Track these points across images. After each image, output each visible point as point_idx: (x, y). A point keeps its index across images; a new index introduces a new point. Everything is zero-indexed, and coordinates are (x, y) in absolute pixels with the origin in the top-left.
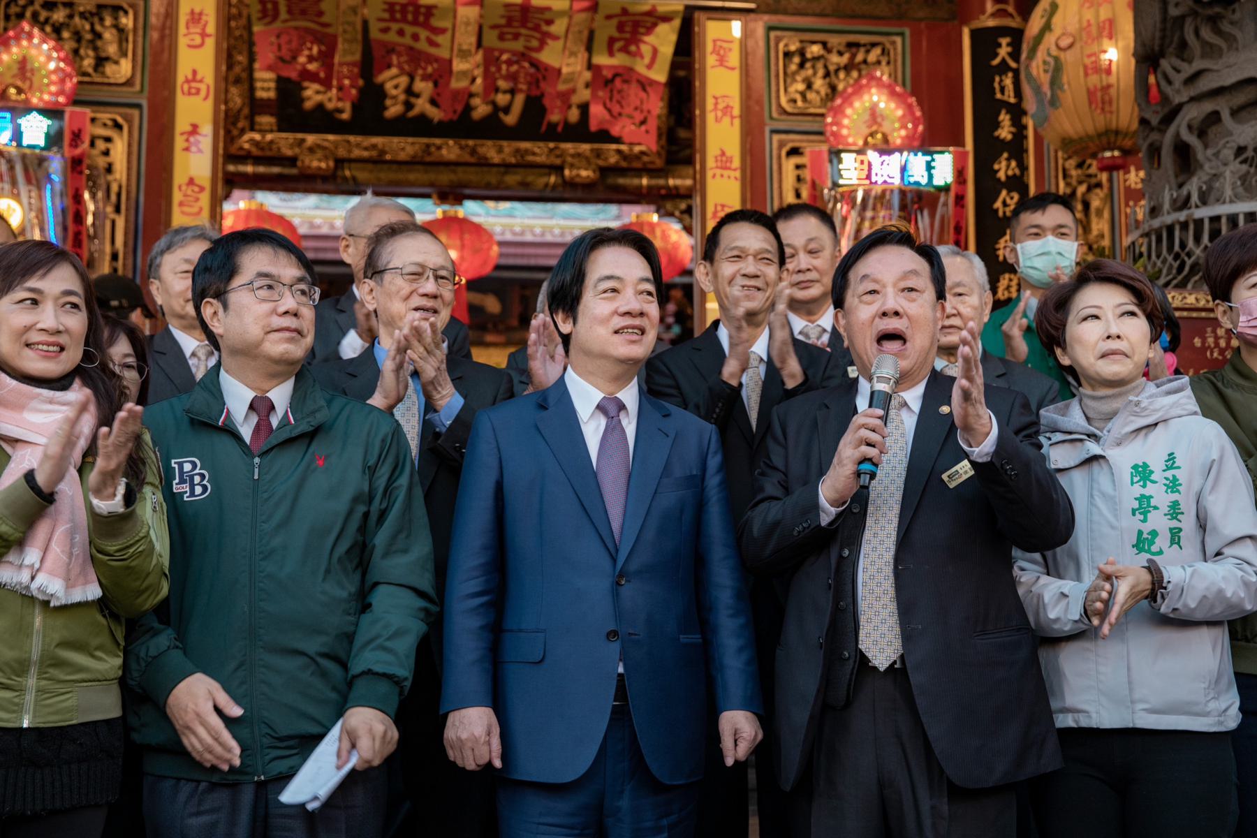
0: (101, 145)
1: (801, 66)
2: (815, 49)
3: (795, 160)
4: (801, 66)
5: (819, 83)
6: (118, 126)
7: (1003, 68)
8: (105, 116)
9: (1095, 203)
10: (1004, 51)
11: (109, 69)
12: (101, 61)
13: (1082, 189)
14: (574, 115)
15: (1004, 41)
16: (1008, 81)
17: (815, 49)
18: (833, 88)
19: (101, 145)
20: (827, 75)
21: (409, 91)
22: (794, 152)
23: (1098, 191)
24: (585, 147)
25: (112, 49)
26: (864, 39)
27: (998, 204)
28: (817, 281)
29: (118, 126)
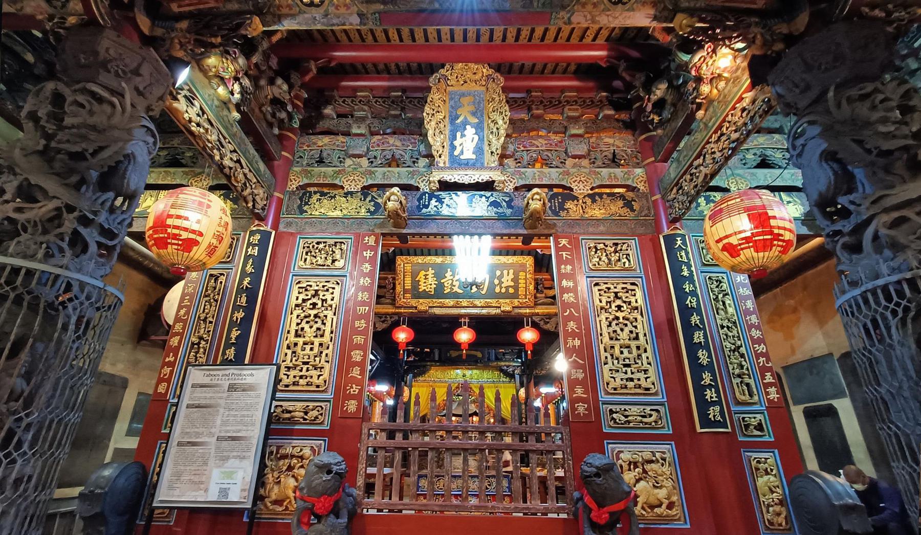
0: (331, 290)
1: (596, 252)
2: (602, 246)
3: (597, 288)
4: (596, 252)
5: (604, 258)
6: (338, 284)
7: (680, 248)
8: (333, 280)
9: (727, 302)
10: (679, 242)
11: (336, 263)
12: (334, 261)
13: (720, 296)
14: (503, 290)
15: (679, 239)
16: (683, 254)
17: (602, 246)
18: (610, 260)
19: (331, 290)
20: (607, 255)
21: (452, 284)
22: (597, 284)
23: (517, 439)
24: (508, 301)
25: (338, 257)
26: (619, 242)
27: (688, 302)
28: (460, 477)
29: (338, 284)
